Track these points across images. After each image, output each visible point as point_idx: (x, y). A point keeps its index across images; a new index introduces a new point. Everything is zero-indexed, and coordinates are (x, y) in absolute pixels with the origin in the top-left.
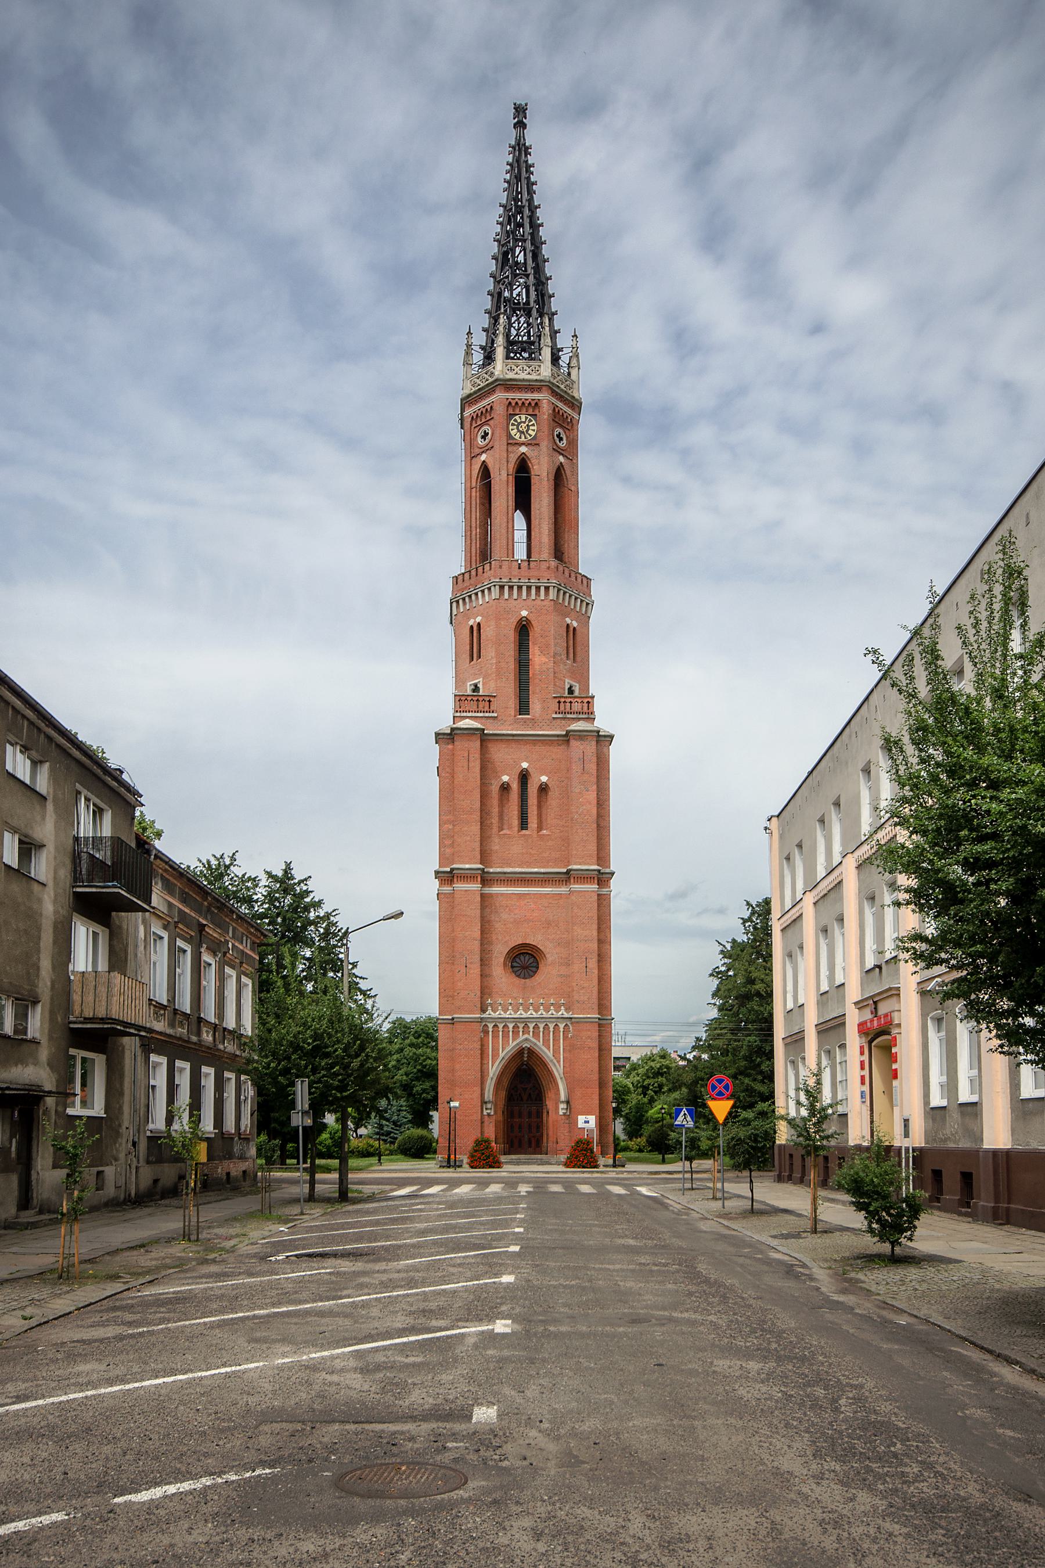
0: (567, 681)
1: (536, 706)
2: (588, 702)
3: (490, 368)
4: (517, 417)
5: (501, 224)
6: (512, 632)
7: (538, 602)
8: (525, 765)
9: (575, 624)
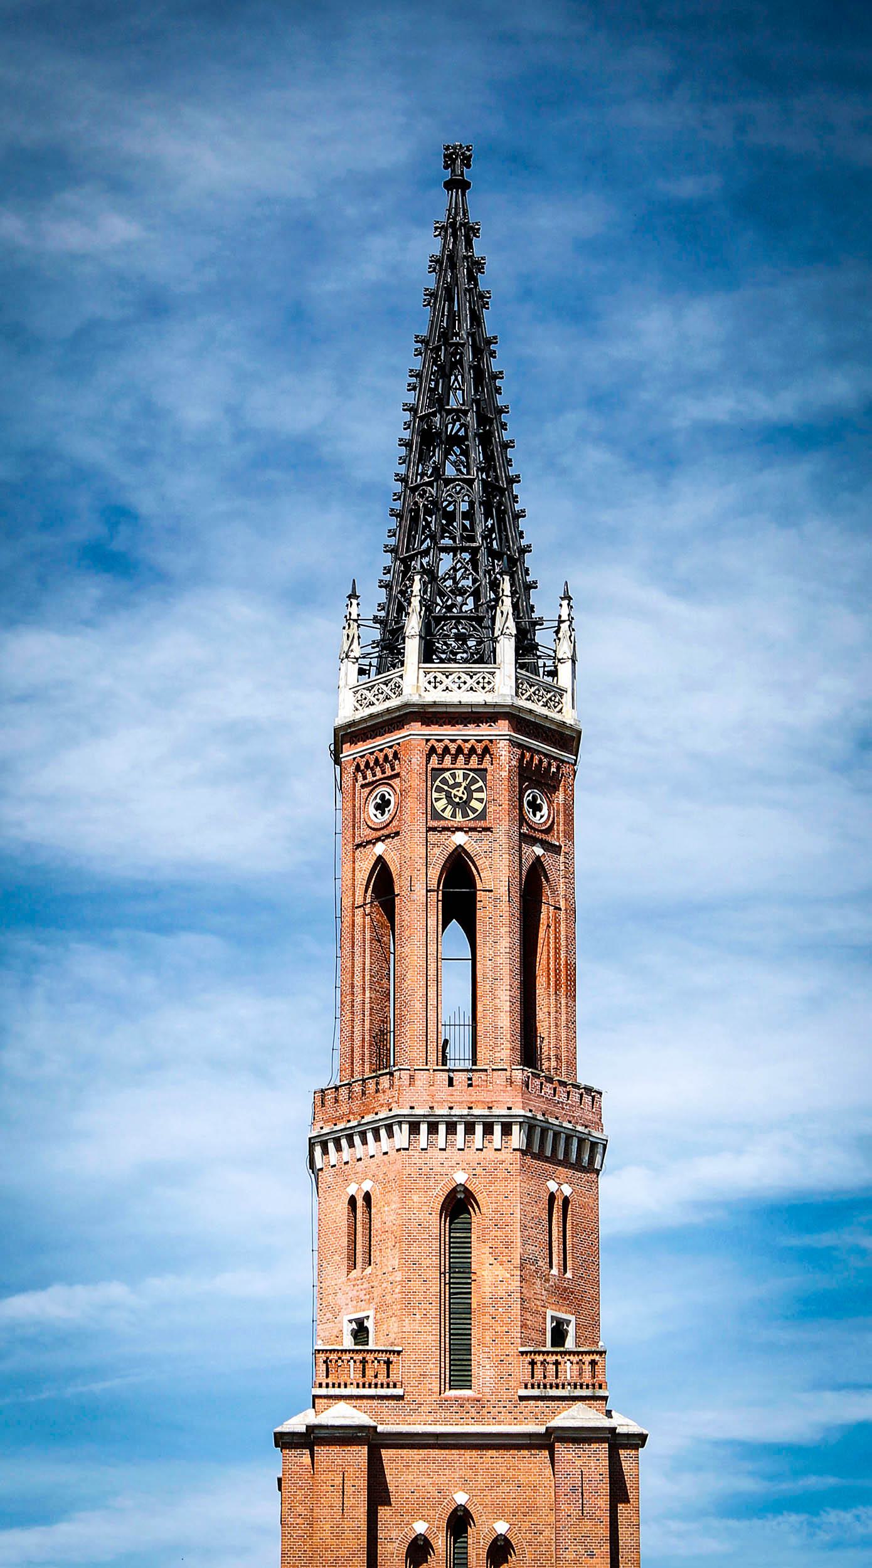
0: (550, 1313)
1: (483, 1370)
2: (593, 1363)
3: (394, 673)
4: (447, 775)
5: (394, 550)
6: (435, 1217)
7: (489, 1154)
8: (461, 1498)
9: (567, 1190)
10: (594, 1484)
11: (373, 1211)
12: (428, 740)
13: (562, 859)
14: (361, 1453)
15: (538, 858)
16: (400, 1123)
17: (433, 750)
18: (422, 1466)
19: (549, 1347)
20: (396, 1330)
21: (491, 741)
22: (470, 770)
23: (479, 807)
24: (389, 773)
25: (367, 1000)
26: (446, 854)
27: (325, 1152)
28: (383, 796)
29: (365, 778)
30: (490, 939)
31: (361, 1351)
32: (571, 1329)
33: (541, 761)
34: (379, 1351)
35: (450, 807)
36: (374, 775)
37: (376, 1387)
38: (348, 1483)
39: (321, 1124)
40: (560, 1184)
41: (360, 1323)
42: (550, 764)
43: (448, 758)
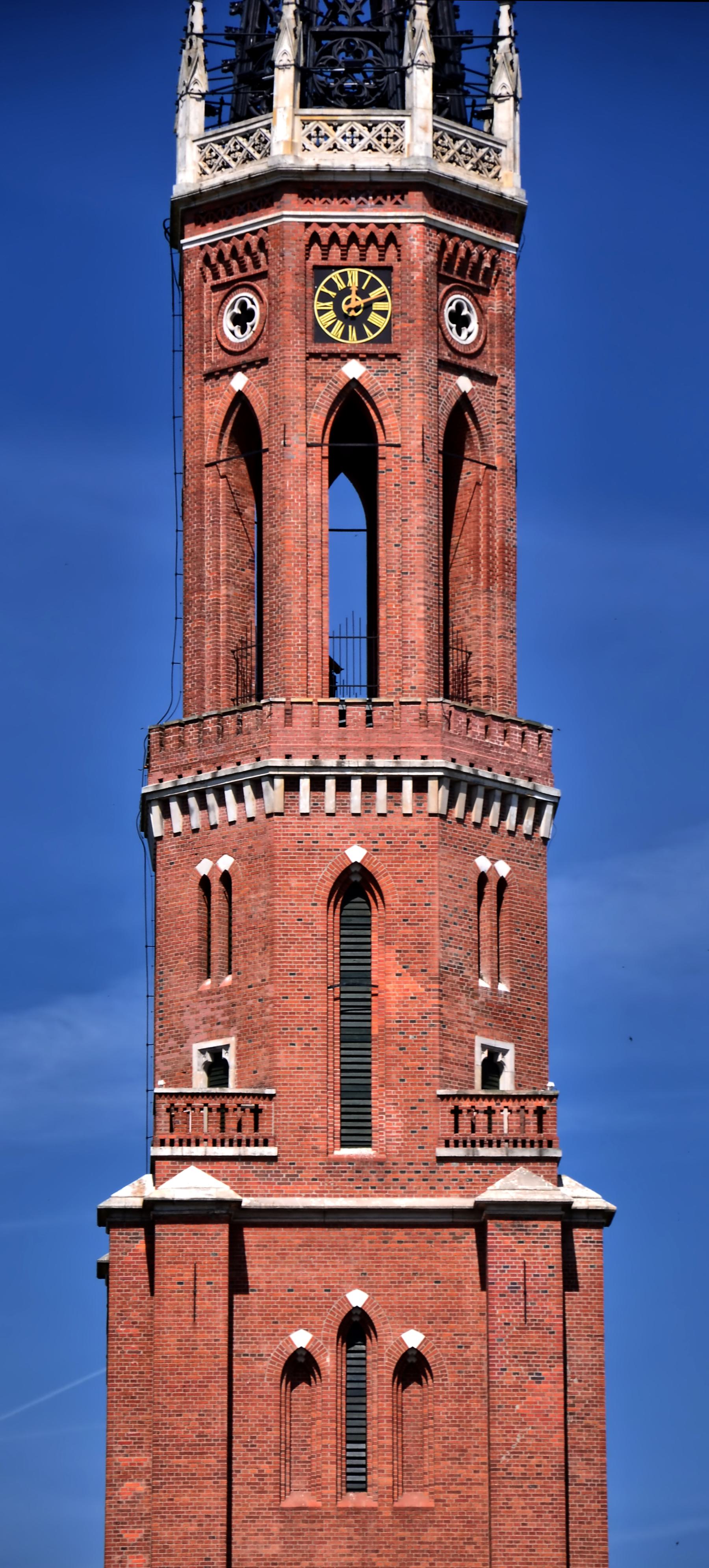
0: (479, 1040)
1: (388, 1119)
3: (256, 123)
4: (335, 276)
6: (321, 907)
7: (395, 821)
9: (503, 869)
10: (542, 1280)
11: (234, 898)
12: (308, 225)
13: (497, 396)
14: (220, 1234)
15: (464, 395)
16: (271, 778)
17: (315, 238)
18: (304, 1254)
19: (478, 1090)
20: (267, 1066)
21: (398, 226)
22: (368, 268)
23: (381, 322)
24: (251, 271)
25: (223, 600)
26: (334, 392)
27: (166, 814)
28: (243, 305)
29: (216, 276)
30: (396, 516)
31: (218, 1095)
32: (509, 1061)
33: (469, 253)
34: (243, 1095)
35: (339, 323)
36: (229, 272)
37: (239, 1145)
38: (202, 1280)
39: (160, 775)
40: (493, 861)
41: (216, 1053)
42: (481, 257)
43: (335, 251)
